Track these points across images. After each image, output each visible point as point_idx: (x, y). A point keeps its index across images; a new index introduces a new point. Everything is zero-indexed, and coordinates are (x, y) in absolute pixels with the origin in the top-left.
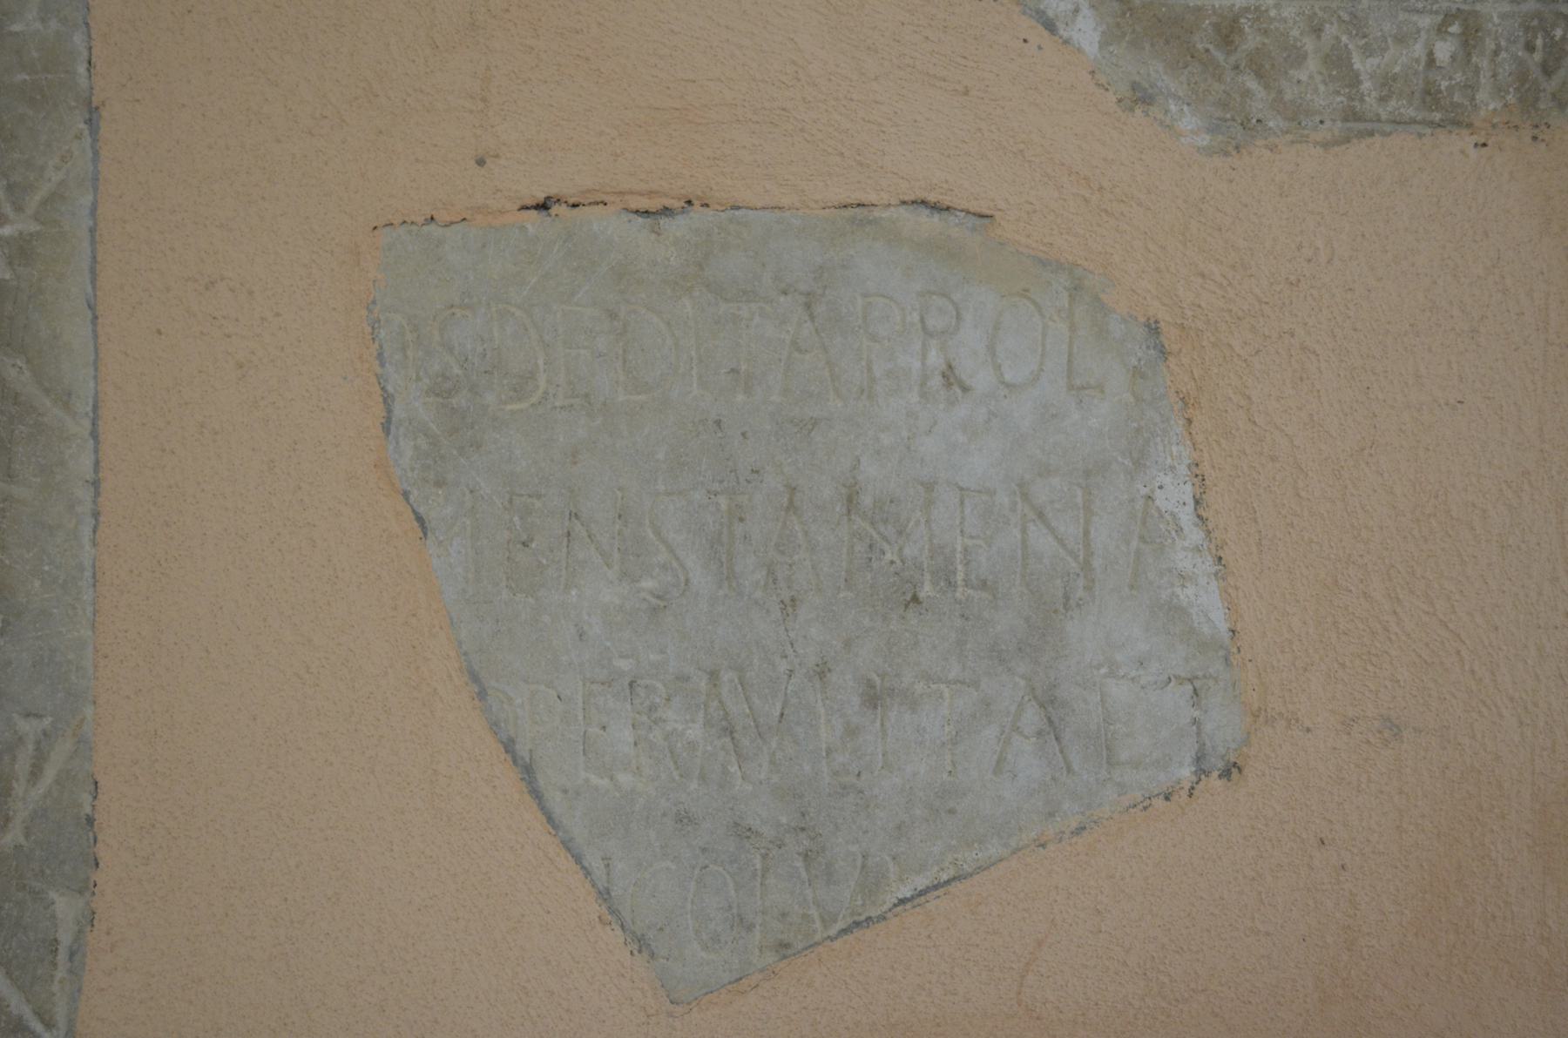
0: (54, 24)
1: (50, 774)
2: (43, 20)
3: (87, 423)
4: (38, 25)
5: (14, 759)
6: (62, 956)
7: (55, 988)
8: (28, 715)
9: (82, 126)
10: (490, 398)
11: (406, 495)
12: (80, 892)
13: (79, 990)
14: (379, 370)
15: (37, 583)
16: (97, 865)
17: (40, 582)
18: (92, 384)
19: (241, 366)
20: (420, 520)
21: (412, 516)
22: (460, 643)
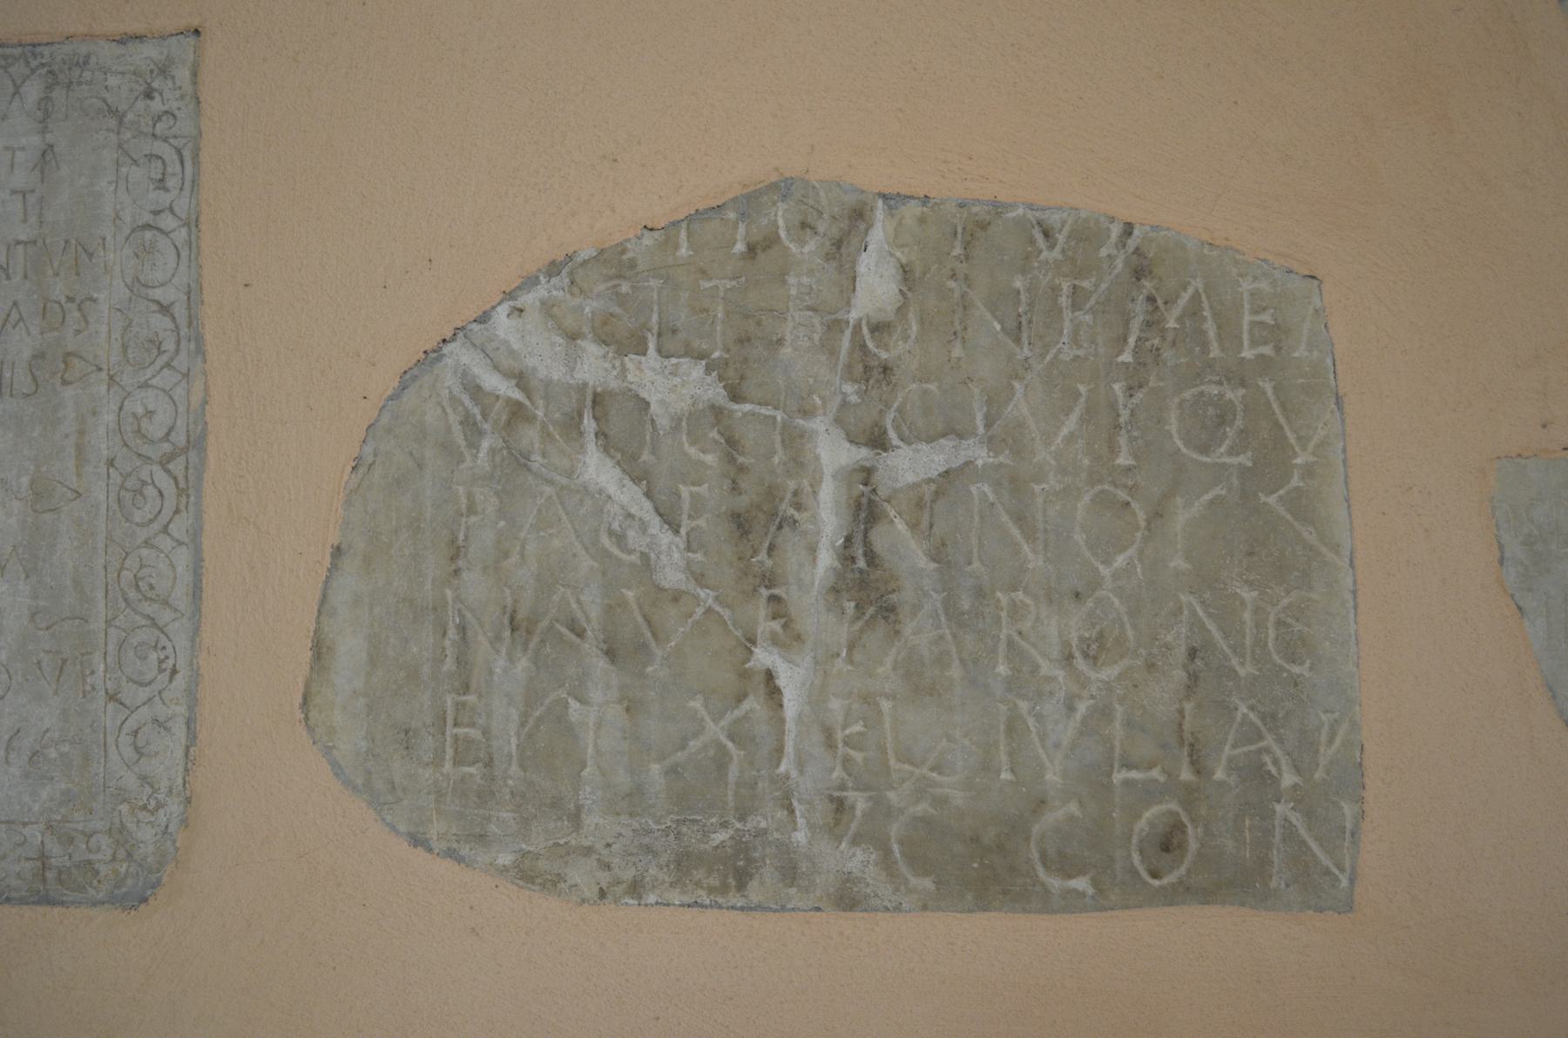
0: (1316, 353)
1: (1338, 741)
2: (1309, 351)
3: (1347, 560)
4: (1306, 353)
5: (1320, 734)
6: (1348, 835)
7: (1345, 851)
8: (1327, 712)
9: (1333, 406)
10: (1553, 547)
11: (1512, 596)
12: (1357, 802)
13: (1358, 852)
14: (1496, 532)
15: (1328, 643)
16: (1364, 788)
17: (405, 674)
18: (1349, 540)
19: (1426, 531)
20: (1520, 608)
21: (1515, 607)
22: (1542, 671)
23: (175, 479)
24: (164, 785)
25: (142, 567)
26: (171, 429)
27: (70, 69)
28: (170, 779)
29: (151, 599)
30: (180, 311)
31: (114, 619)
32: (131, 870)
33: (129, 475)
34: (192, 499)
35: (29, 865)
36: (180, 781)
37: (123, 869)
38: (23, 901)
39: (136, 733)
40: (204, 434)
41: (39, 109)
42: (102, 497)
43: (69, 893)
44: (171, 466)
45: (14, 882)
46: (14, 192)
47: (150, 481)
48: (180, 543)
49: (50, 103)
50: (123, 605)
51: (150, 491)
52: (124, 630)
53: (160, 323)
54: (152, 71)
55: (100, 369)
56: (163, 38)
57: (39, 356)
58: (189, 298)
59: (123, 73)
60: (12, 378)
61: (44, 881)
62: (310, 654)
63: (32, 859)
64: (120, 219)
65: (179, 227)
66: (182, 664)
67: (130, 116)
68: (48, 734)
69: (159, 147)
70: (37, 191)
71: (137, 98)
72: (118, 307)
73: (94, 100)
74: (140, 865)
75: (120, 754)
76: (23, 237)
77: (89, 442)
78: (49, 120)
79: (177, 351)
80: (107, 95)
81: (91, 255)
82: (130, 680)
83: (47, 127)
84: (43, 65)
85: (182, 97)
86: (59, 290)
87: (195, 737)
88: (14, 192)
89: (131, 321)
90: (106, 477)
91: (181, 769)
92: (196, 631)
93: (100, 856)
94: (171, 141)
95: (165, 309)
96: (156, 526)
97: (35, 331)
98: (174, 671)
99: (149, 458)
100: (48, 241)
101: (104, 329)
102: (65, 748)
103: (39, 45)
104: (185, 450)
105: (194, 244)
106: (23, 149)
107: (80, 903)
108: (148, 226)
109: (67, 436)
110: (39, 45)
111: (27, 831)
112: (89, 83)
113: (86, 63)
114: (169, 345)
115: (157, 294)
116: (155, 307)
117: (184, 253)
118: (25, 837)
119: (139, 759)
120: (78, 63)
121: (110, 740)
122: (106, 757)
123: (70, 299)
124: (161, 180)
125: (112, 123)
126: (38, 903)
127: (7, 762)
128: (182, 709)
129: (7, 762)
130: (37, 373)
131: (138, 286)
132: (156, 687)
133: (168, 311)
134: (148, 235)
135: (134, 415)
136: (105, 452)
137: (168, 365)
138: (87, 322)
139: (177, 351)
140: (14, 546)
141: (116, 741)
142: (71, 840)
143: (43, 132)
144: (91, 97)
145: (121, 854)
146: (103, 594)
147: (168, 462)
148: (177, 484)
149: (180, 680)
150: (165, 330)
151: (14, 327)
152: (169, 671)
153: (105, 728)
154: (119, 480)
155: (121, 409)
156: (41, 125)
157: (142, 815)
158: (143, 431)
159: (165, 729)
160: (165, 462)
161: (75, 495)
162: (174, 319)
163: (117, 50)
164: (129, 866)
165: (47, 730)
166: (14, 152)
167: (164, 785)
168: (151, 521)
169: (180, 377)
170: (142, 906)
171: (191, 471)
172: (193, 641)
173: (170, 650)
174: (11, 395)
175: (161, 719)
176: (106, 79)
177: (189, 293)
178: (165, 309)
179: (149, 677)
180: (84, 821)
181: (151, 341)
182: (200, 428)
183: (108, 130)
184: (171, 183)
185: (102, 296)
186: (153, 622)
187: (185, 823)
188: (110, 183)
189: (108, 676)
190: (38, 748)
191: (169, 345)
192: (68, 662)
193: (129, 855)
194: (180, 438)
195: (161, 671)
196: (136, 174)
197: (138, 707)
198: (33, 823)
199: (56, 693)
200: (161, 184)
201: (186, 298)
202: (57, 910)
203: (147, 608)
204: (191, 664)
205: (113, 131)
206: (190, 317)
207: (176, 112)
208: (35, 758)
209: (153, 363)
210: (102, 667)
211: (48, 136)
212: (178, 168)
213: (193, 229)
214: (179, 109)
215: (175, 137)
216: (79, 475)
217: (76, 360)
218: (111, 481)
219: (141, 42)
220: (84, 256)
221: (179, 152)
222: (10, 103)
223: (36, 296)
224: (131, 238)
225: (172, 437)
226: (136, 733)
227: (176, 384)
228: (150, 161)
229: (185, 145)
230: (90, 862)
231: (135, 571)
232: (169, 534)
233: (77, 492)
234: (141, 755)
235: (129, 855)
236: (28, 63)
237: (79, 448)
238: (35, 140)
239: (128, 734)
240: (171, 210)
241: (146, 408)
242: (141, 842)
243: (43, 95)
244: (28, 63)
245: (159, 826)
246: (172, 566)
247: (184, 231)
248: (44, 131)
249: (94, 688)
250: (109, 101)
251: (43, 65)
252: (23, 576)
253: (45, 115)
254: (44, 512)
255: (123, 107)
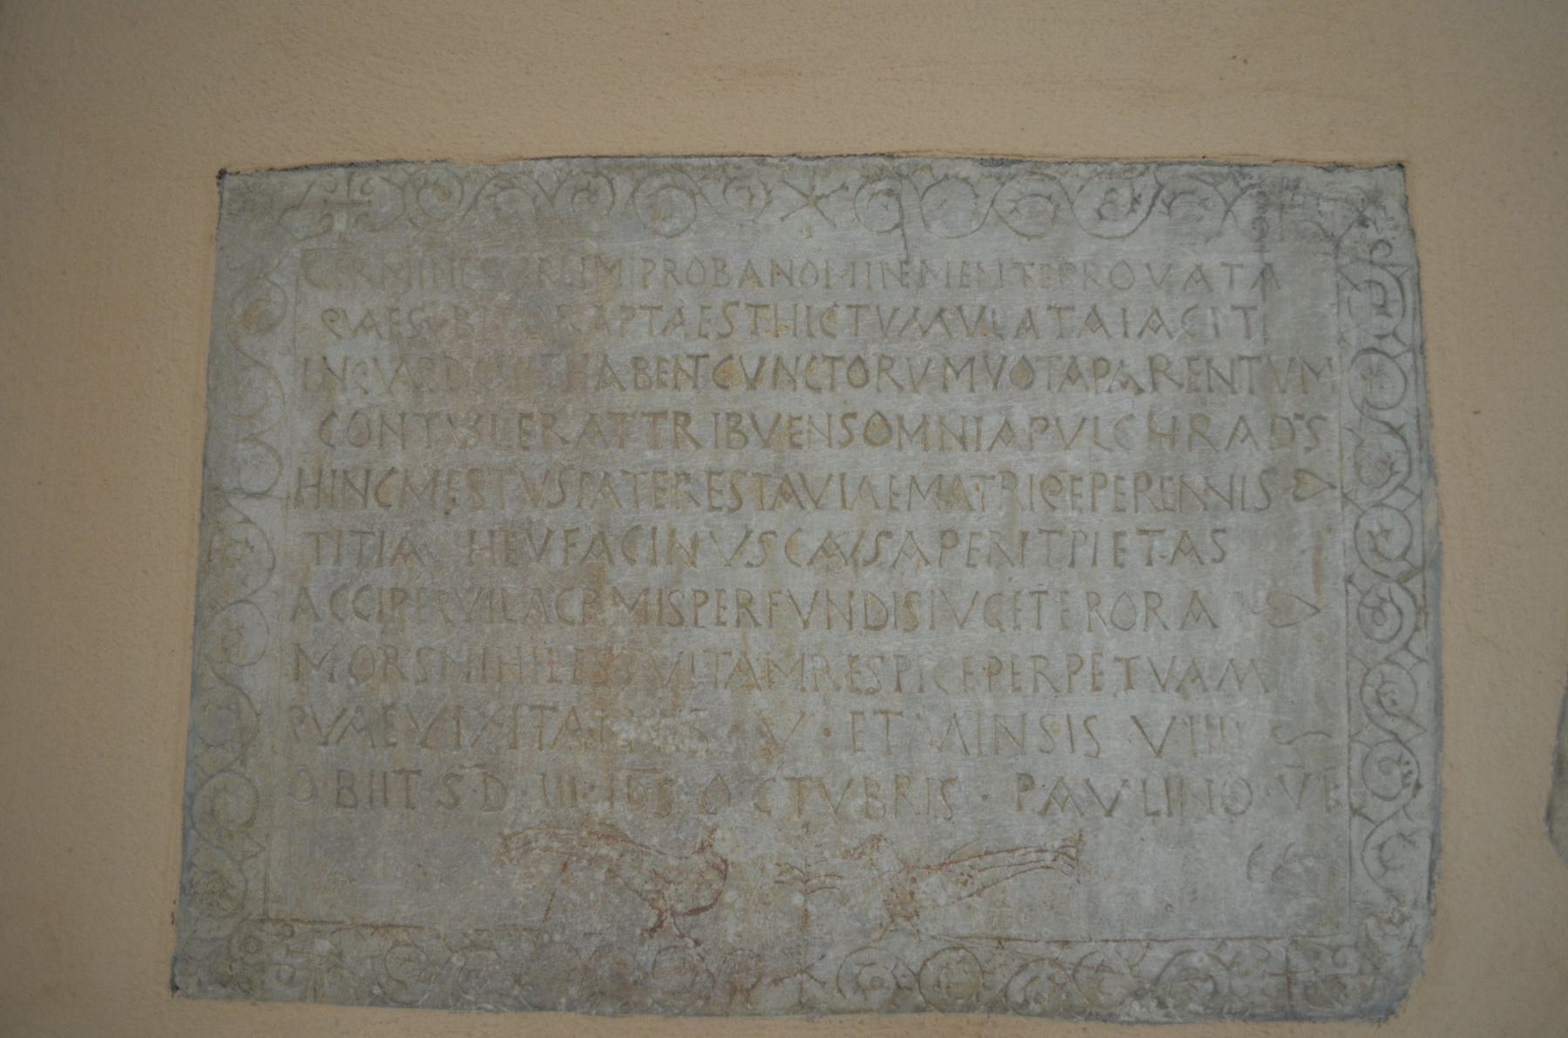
23: (1413, 597)
24: (1410, 897)
25: (1384, 683)
26: (1408, 548)
27: (1280, 192)
28: (1415, 892)
29: (1395, 715)
30: (1410, 433)
31: (1356, 734)
32: (1379, 983)
33: (1368, 592)
34: (1431, 617)
35: (1274, 981)
36: (1424, 894)
37: (1369, 983)
38: (1268, 1018)
39: (1381, 847)
40: (1439, 552)
41: (1254, 228)
42: (1342, 613)
43: (1315, 1008)
44: (1409, 585)
45: (1258, 999)
46: (1234, 308)
47: (1389, 599)
48: (1421, 660)
49: (1264, 224)
50: (1365, 720)
51: (1389, 609)
52: (1367, 746)
53: (1391, 444)
54: (1363, 200)
55: (1333, 487)
56: (1370, 169)
57: (1270, 471)
58: (1418, 421)
59: (1335, 200)
60: (1243, 492)
61: (1290, 996)
62: (1551, 769)
63: (1277, 975)
64: (1345, 341)
65: (1404, 352)
66: (1425, 780)
67: (1346, 242)
68: (1292, 849)
69: (1379, 275)
70: (1259, 308)
71: (1350, 226)
72: (1348, 426)
73: (1309, 224)
74: (1388, 979)
75: (1366, 868)
76: (1248, 353)
77: (1326, 559)
78: (1265, 240)
79: (1410, 473)
80: (1322, 220)
81: (1317, 375)
82: (1374, 794)
83: (1264, 246)
84: (1252, 186)
85: (1396, 227)
86: (1287, 407)
87: (1440, 850)
88: (1234, 308)
89: (1362, 442)
90: (1344, 593)
91: (1425, 881)
92: (1439, 746)
93: (1347, 970)
94: (1390, 269)
95: (1395, 431)
96: (1397, 643)
97: (1264, 446)
98: (1418, 786)
99: (1386, 576)
100: (1274, 358)
101: (1336, 447)
102: (1310, 863)
103: (1247, 166)
104: (1423, 568)
105: (1421, 370)
106: (1241, 266)
107: (1327, 1018)
108: (1373, 350)
109: (1303, 552)
110: (1247, 166)
111: (1271, 947)
112: (1302, 206)
113: (1296, 187)
114: (1402, 467)
115: (1387, 415)
116: (1386, 429)
117: (1411, 379)
118: (1269, 953)
119: (1384, 873)
120: (1287, 187)
121: (1356, 854)
122: (1351, 871)
123: (1298, 416)
124: (1382, 306)
125: (1329, 247)
126: (1286, 1018)
127: (1249, 877)
128: (1426, 823)
129: (1249, 877)
130: (1270, 489)
131: (1368, 407)
132: (1401, 801)
133: (1397, 433)
134: (1375, 358)
135: (1370, 532)
136: (1343, 569)
137: (1401, 486)
138: (1317, 439)
139: (1410, 473)
140: (1252, 661)
141: (1362, 856)
142: (1317, 955)
143: (1261, 251)
144: (1306, 220)
145: (1368, 968)
146: (1346, 709)
147: (1407, 579)
148: (1415, 602)
149: (1425, 796)
150: (1397, 451)
151: (1243, 441)
152: (1412, 785)
153: (1350, 842)
154: (1358, 597)
155: (1357, 526)
156: (1258, 244)
157: (1389, 928)
158: (1380, 550)
159: (1410, 842)
160: (1402, 580)
161: (1314, 610)
162: (1404, 440)
163: (1328, 177)
164: (1375, 980)
165: (1291, 845)
166: (1232, 270)
167: (1410, 897)
168: (1392, 638)
169: (1413, 498)
170: (1392, 1018)
171: (1429, 590)
172: (1436, 756)
173: (1413, 766)
174: (1243, 509)
175: (1407, 834)
176: (1318, 205)
177: (1418, 416)
178: (1395, 431)
179: (1394, 791)
180: (1329, 935)
181: (1383, 462)
182: (1435, 548)
183: (1326, 254)
184: (1394, 309)
185: (1332, 416)
186: (1396, 737)
187: (1430, 935)
188: (1333, 305)
189: (1352, 790)
190: (1281, 862)
191: (1402, 467)
192: (1312, 777)
193: (1376, 968)
194: (1416, 557)
195: (1405, 785)
196: (1358, 298)
197: (1383, 822)
198: (1277, 939)
199: (1298, 807)
200: (1383, 309)
201: (1415, 421)
202: (1305, 1027)
203: (1392, 724)
204: (1435, 779)
205: (1330, 255)
206: (1420, 439)
207: (1392, 242)
208: (1279, 872)
209: (1387, 482)
210: (1346, 782)
211: (1266, 255)
212: (1398, 296)
213: (1419, 355)
214: (1394, 238)
215: (1393, 265)
216: (1318, 591)
217: (1308, 477)
218: (1350, 598)
219: (1348, 171)
220: (1311, 376)
221: (1398, 280)
222: (1224, 219)
223: (1263, 412)
224: (1358, 360)
225: (1409, 556)
226: (1381, 847)
227: (1410, 505)
228: (1370, 287)
229: (1404, 273)
230: (1336, 977)
231: (1376, 687)
232: (1409, 651)
233: (1316, 608)
234: (1386, 868)
235: (1376, 968)
236: (1237, 183)
237: (1317, 564)
238: (1253, 259)
239: (1373, 848)
240: (1394, 334)
241: (1381, 526)
242: (1388, 955)
243: (1257, 215)
244: (1237, 183)
245: (1405, 938)
246: (1414, 683)
247: (1410, 356)
248: (1262, 250)
249: (1338, 803)
250: (1324, 226)
251: (1252, 186)
252: (1262, 690)
253: (1260, 234)
254: (1282, 626)
255: (1339, 232)
